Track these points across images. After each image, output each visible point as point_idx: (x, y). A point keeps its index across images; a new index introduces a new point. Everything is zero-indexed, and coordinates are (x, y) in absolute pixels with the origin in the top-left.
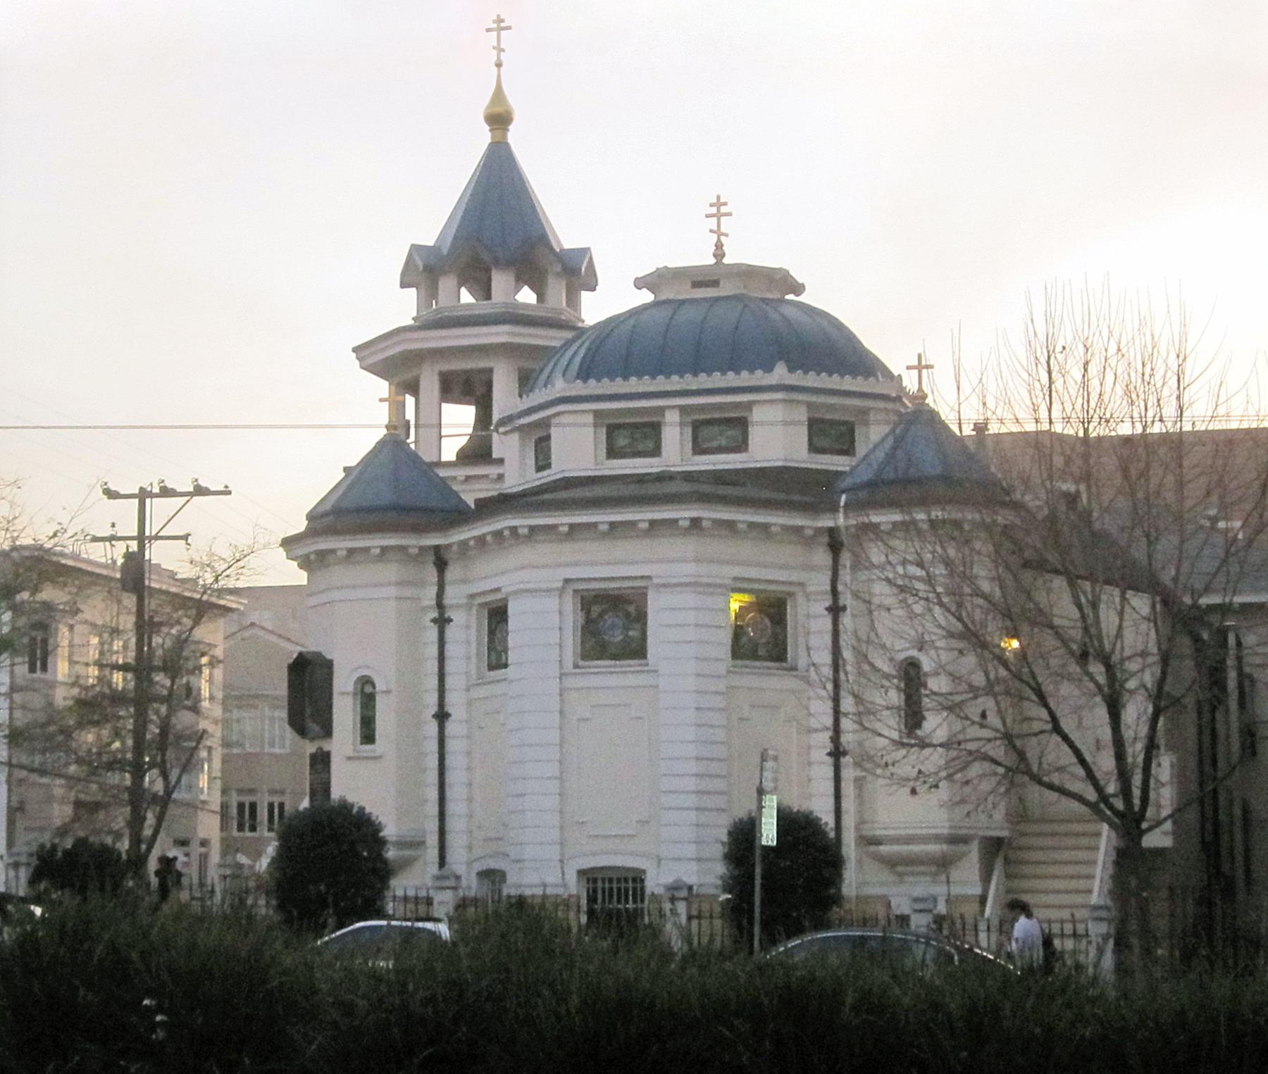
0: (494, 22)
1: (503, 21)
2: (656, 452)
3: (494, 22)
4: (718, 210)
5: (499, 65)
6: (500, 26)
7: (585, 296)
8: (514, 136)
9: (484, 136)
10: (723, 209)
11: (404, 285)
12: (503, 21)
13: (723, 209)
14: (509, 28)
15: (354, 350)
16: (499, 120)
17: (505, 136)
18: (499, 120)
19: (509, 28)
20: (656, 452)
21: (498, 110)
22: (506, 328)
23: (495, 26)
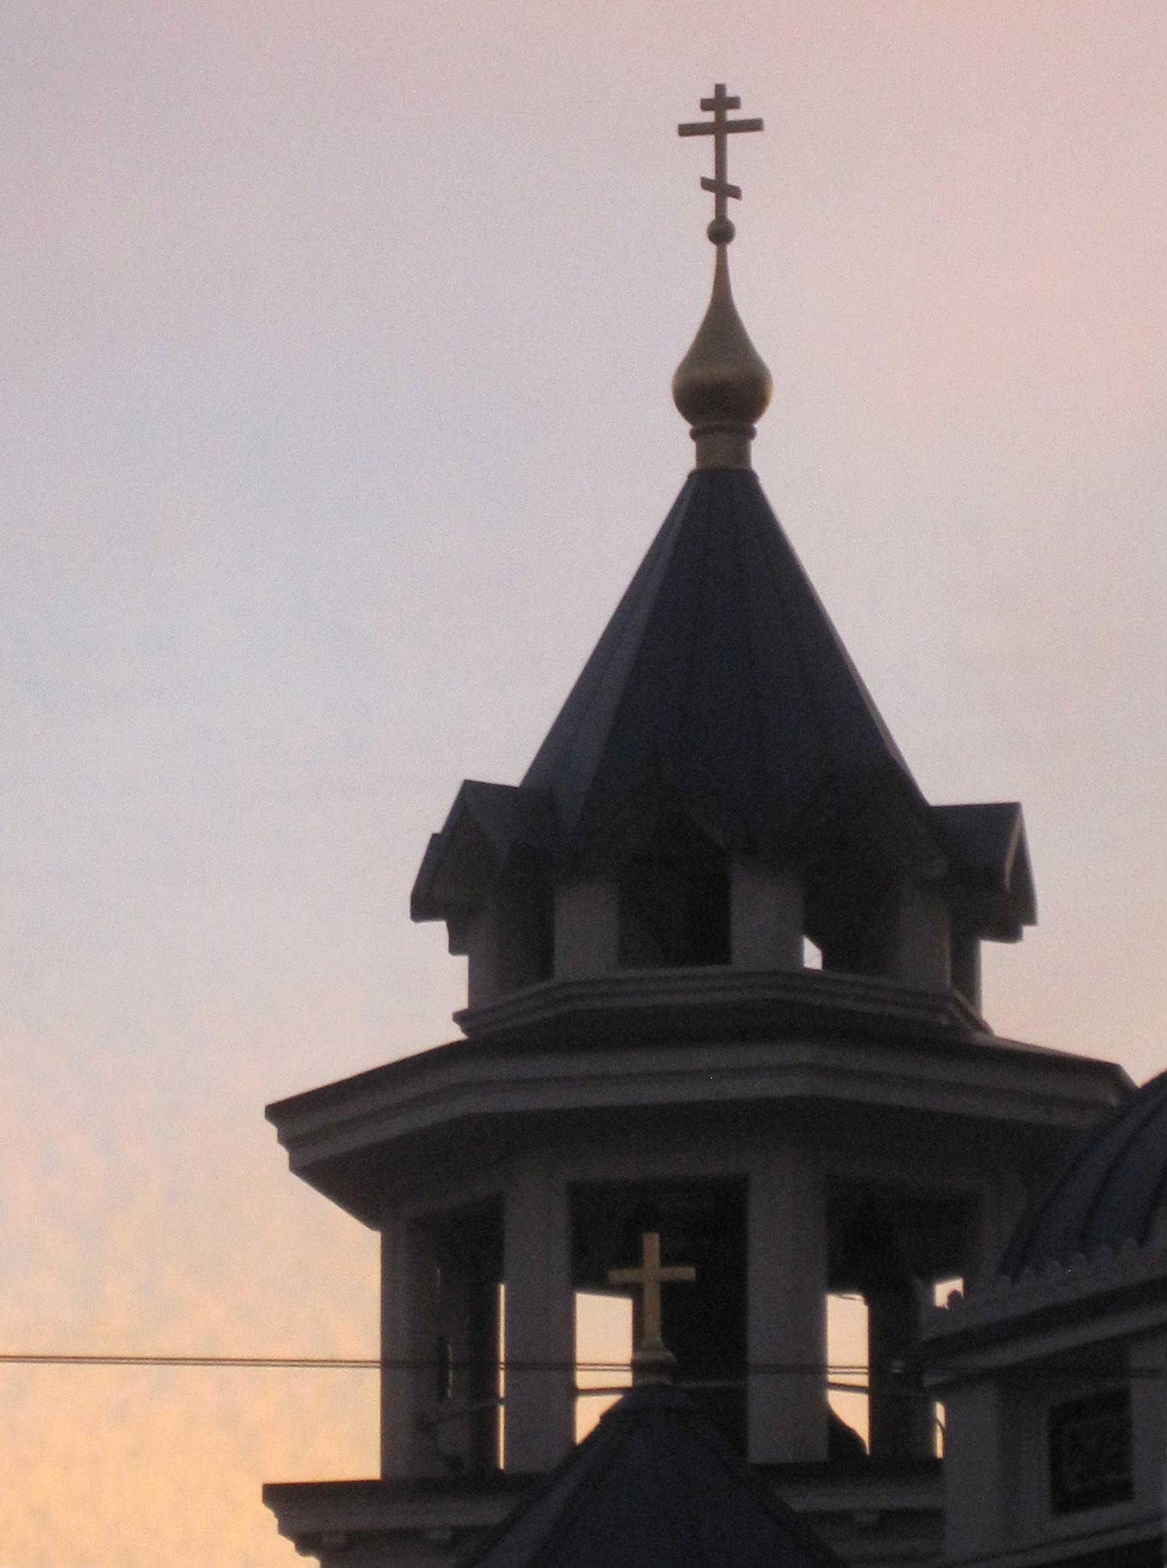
0: (706, 105)
1: (734, 103)
2: (1123, 1492)
3: (706, 105)
4: (720, 117)
5: (721, 233)
6: (721, 118)
7: (991, 953)
8: (775, 455)
9: (673, 454)
10: (732, 115)
11: (423, 906)
12: (734, 103)
13: (732, 115)
14: (754, 125)
15: (277, 1112)
16: (722, 391)
17: (742, 454)
18: (722, 391)
19: (754, 125)
20: (1123, 1492)
21: (722, 371)
22: (803, 1053)
23: (709, 117)
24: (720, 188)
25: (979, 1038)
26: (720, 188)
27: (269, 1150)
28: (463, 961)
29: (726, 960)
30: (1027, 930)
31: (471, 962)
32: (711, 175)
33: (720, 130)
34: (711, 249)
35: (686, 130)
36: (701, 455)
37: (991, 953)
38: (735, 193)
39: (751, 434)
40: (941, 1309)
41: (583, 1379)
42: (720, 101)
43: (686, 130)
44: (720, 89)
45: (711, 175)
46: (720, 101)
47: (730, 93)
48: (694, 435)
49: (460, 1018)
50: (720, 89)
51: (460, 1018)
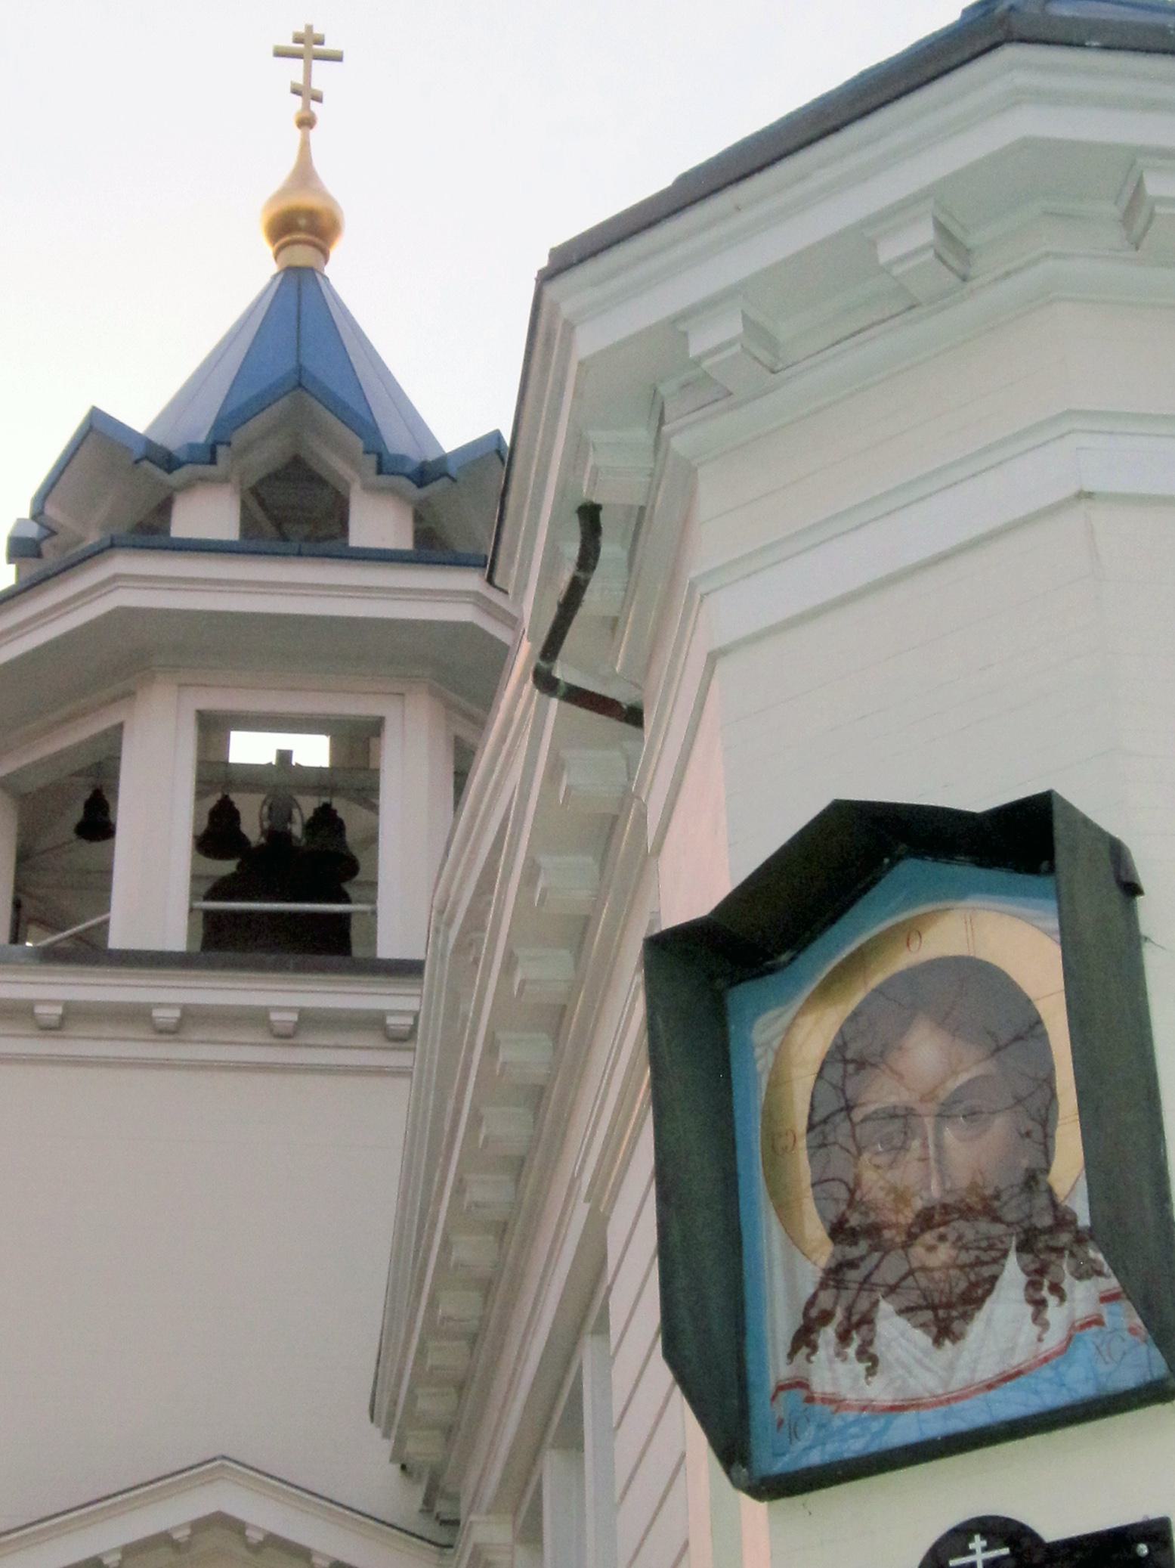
0: (298, 39)
5: (306, 122)
8: (346, 273)
9: (258, 267)
14: (337, 57)
16: (303, 228)
18: (303, 228)
19: (337, 57)
26: (305, 92)
27: (1145, 890)
28: (13, 567)
31: (320, 770)
34: (297, 133)
40: (261, 847)
44: (309, 28)
47: (316, 31)
50: (309, 28)
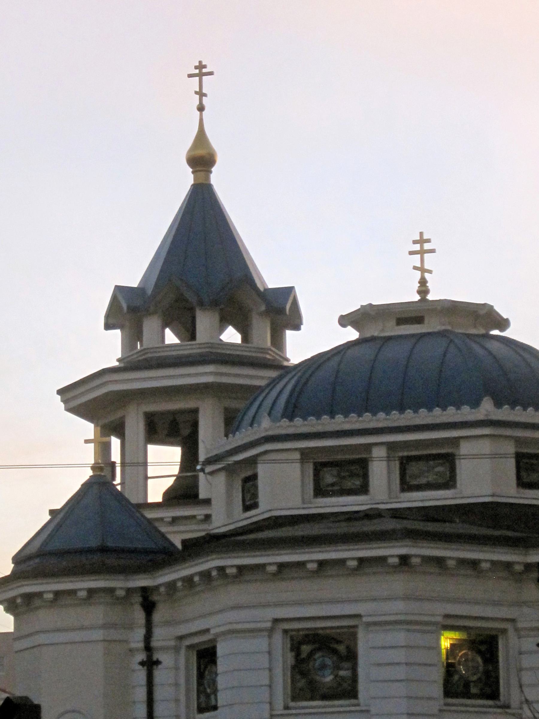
0: (196, 68)
1: (205, 67)
3: (196, 68)
4: (200, 71)
5: (201, 108)
6: (201, 71)
7: (289, 334)
8: (218, 178)
9: (187, 179)
10: (204, 70)
12: (205, 67)
13: (204, 70)
14: (211, 73)
15: (60, 392)
16: (202, 160)
18: (202, 160)
19: (211, 73)
21: (200, 152)
23: (197, 71)
24: (201, 94)
25: (286, 364)
26: (201, 94)
28: (117, 333)
29: (198, 651)
30: (302, 326)
32: (198, 90)
33: (201, 75)
34: (198, 113)
35: (190, 76)
36: (195, 179)
37: (289, 334)
38: (205, 95)
39: (211, 172)
41: (151, 471)
42: (201, 66)
43: (190, 76)
44: (200, 62)
45: (198, 90)
46: (201, 66)
48: (193, 172)
49: (118, 360)
50: (200, 62)
51: (118, 360)
